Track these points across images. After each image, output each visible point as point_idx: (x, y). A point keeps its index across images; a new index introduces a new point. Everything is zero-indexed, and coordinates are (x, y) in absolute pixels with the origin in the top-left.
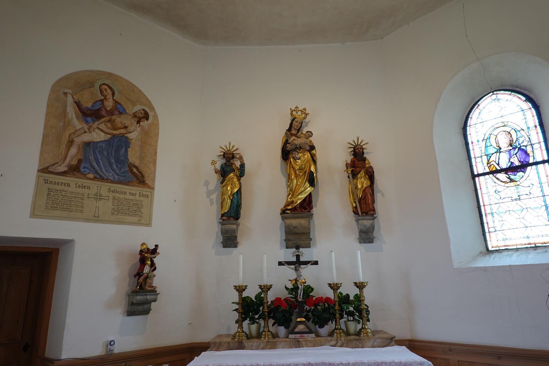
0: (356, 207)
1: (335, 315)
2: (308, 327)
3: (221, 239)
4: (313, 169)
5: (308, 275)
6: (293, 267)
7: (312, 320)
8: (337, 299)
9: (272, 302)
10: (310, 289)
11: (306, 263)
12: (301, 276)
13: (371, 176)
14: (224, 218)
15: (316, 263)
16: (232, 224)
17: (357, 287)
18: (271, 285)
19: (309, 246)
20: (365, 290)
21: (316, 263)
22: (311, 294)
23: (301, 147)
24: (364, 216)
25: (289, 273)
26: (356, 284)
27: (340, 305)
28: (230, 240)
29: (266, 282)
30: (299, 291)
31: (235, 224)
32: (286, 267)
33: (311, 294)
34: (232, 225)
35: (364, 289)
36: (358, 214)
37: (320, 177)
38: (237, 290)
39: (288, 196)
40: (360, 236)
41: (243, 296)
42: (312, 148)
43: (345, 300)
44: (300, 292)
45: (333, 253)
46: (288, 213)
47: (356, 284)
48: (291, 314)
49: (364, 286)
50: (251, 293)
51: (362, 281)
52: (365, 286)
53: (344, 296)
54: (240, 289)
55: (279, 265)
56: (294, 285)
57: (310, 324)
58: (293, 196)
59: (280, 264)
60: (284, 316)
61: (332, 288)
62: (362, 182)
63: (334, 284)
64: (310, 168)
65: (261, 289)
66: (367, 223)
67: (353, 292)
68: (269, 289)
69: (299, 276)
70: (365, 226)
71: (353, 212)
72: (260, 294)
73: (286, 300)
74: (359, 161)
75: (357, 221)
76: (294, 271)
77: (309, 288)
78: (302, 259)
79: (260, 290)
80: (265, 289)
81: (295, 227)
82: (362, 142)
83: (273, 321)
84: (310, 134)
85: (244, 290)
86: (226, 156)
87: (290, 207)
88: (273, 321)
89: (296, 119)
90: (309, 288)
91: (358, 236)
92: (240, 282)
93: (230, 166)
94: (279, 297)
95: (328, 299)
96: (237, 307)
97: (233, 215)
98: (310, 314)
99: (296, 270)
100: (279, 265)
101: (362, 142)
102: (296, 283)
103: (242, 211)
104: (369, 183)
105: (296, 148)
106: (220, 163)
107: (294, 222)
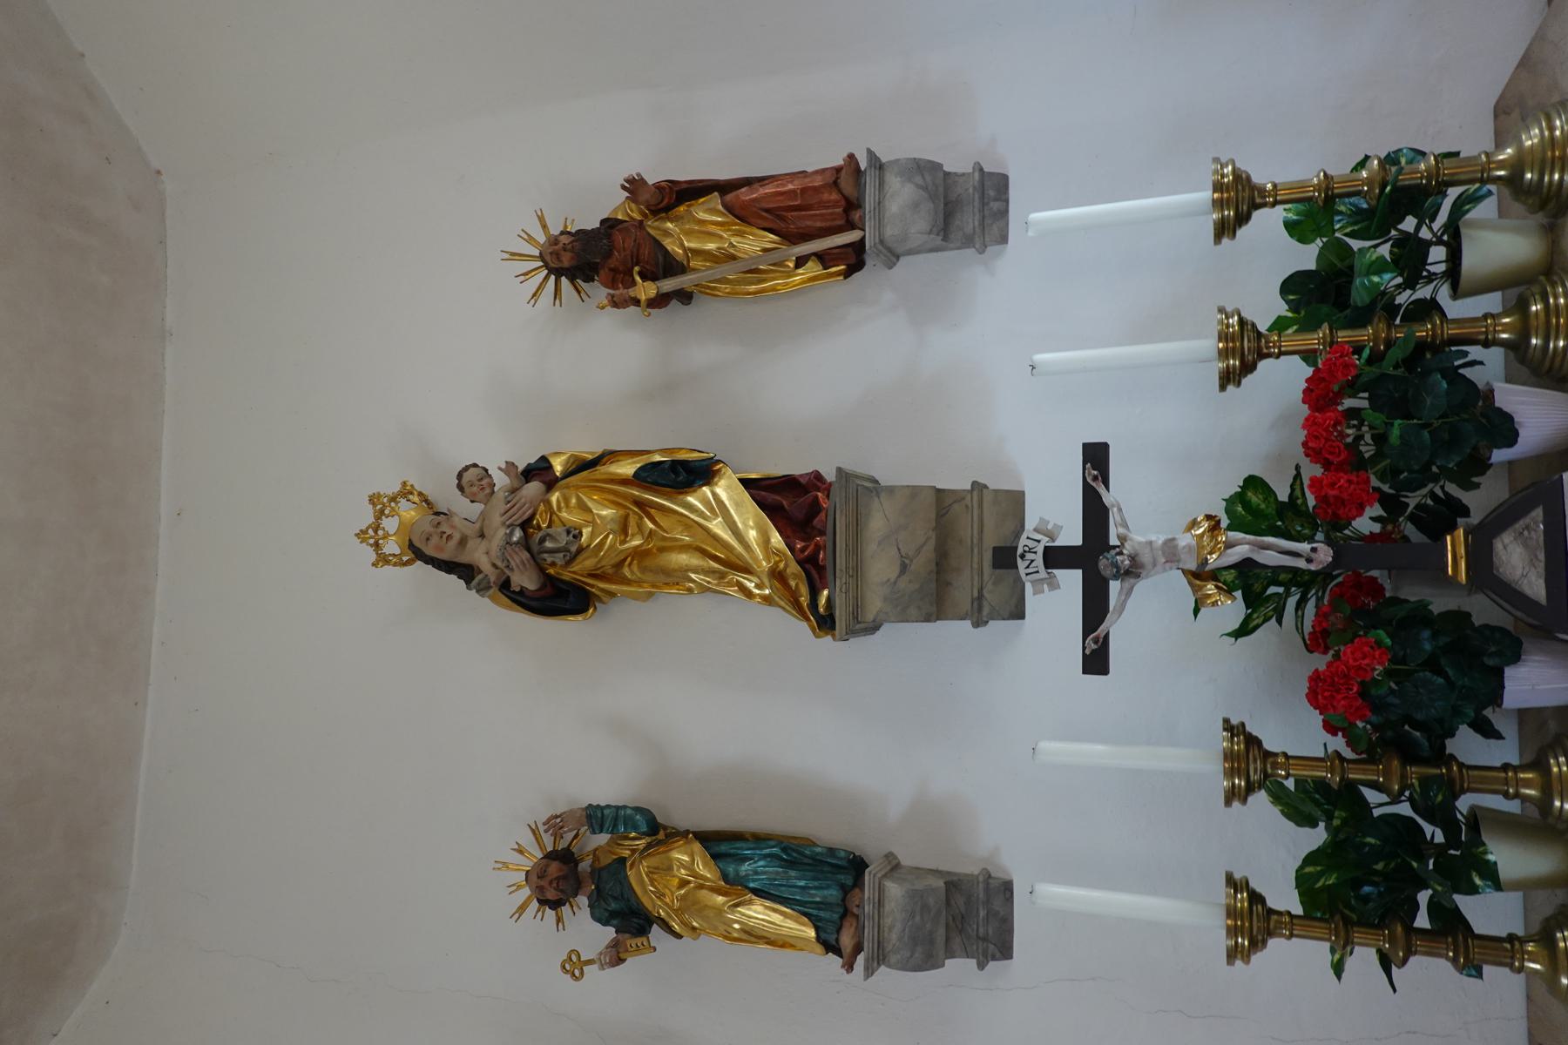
0: (824, 258)
1: (1421, 346)
2: (1502, 519)
3: (959, 968)
4: (627, 469)
5: (1160, 506)
6: (1114, 586)
7: (1452, 489)
8: (1314, 340)
9: (1330, 728)
10: (1254, 498)
11: (1095, 512)
12: (1170, 543)
13: (677, 196)
14: (847, 941)
15: (1096, 456)
16: (880, 903)
17: (1242, 219)
18: (1228, 726)
19: (1015, 502)
20: (1262, 177)
21: (1096, 456)
22: (1283, 496)
23: (525, 525)
24: (862, 218)
25: (1149, 614)
26: (1224, 230)
27: (1360, 318)
28: (971, 917)
29: (1204, 762)
30: (1270, 558)
31: (881, 890)
32: (1120, 632)
33: (1283, 496)
34: (889, 906)
35: (1257, 179)
36: (859, 247)
37: (663, 437)
38: (1257, 944)
39: (748, 594)
40: (968, 242)
41: (1298, 910)
42: (539, 470)
43: (1318, 295)
44: (1273, 552)
45: (1039, 357)
46: (829, 599)
47: (1224, 230)
48: (1420, 616)
49: (1241, 179)
50: (1276, 850)
51: (1206, 195)
52: (1242, 322)
53: (1294, 307)
54: (1252, 923)
55: (1104, 670)
56: (1229, 591)
57: (1480, 500)
58: (747, 570)
59: (1096, 662)
60: (1432, 664)
61: (1248, 368)
62: (696, 234)
63: (1224, 354)
64: (624, 482)
65: (1250, 789)
66: (896, 207)
67: (1272, 252)
68: (1252, 742)
69: (1170, 552)
70: (915, 206)
71: (847, 274)
72: (1279, 796)
73: (1317, 641)
74: (609, 254)
75: (893, 257)
76: (1142, 587)
77: (1246, 505)
78: (1072, 536)
79: (1261, 798)
80: (1249, 766)
81: (904, 568)
82: (530, 240)
83: (1464, 731)
84: (472, 480)
85: (1256, 898)
86: (551, 894)
87: (804, 590)
88: (1464, 731)
89: (417, 544)
90: (1246, 505)
91: (970, 252)
92: (1204, 920)
93: (598, 873)
94: (1304, 687)
95: (1319, 394)
96: (1364, 958)
97: (833, 894)
98: (1412, 500)
99: (1133, 571)
100: (1104, 670)
101: (530, 240)
102: (1214, 576)
103: (829, 831)
104: (715, 200)
105: (526, 542)
106: (587, 931)
107: (880, 569)
